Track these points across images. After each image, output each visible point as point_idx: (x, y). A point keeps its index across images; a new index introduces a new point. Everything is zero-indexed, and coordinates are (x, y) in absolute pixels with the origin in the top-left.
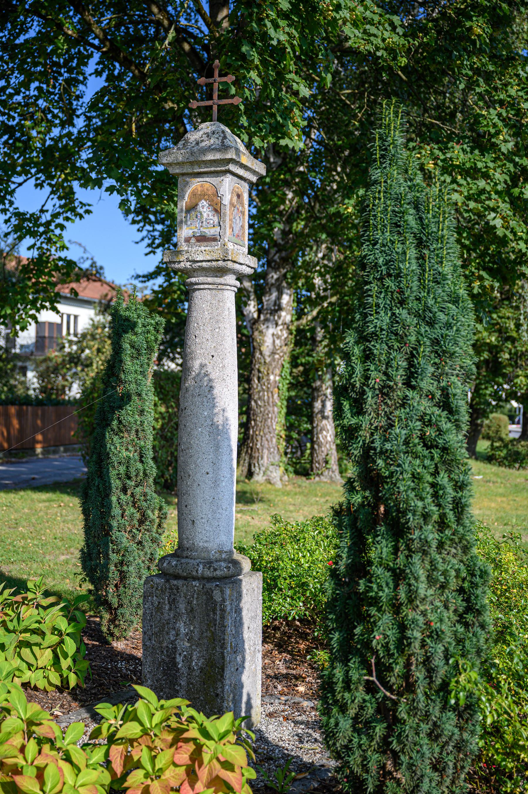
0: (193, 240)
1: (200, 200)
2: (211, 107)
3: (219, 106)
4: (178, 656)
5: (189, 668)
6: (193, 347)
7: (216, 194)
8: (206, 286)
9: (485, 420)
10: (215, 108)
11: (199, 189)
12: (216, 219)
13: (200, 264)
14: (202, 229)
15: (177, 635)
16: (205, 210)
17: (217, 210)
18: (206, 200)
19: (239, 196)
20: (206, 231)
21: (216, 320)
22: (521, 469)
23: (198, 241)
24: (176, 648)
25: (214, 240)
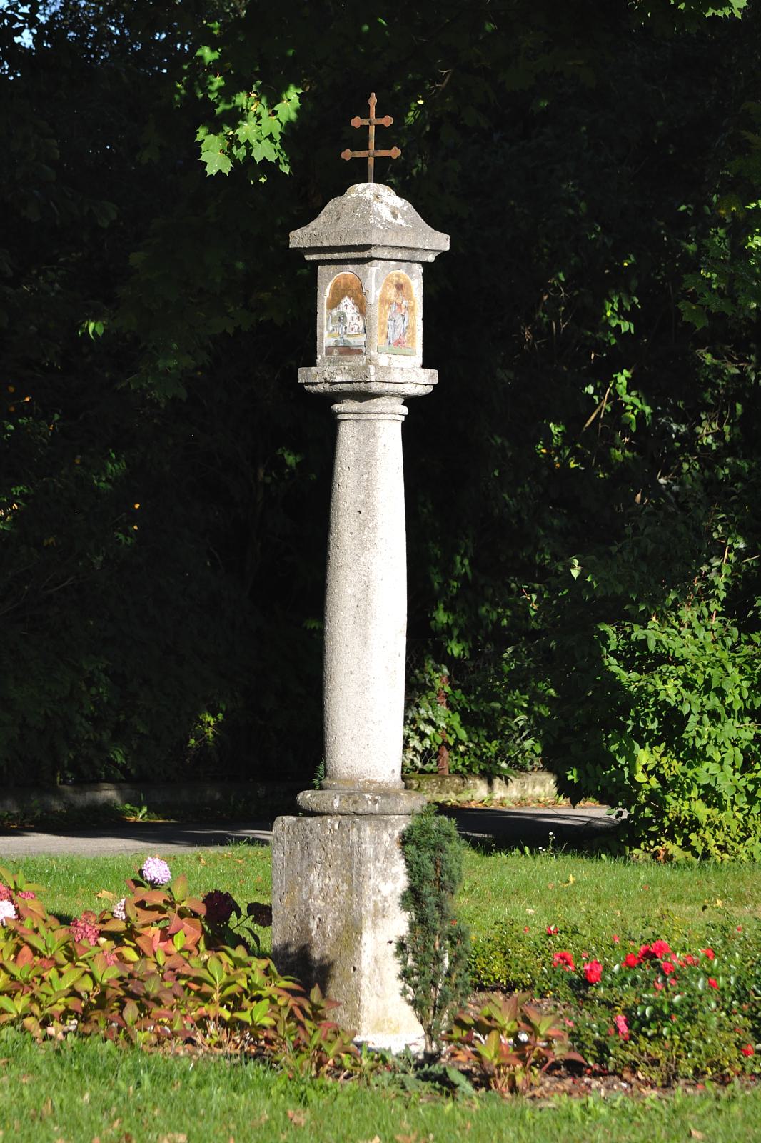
0: (335, 353)
1: (343, 297)
2: (365, 160)
3: (375, 158)
4: (311, 921)
5: (324, 936)
6: (378, 476)
7: (360, 289)
8: (351, 416)
9: (636, 627)
10: (371, 162)
11: (342, 281)
12: (361, 324)
13: (340, 386)
14: (345, 338)
15: (311, 892)
16: (348, 311)
17: (362, 308)
18: (350, 297)
19: (400, 287)
20: (351, 340)
21: (366, 462)
22: (380, 922)
23: (341, 353)
24: (308, 910)
25: (360, 352)
